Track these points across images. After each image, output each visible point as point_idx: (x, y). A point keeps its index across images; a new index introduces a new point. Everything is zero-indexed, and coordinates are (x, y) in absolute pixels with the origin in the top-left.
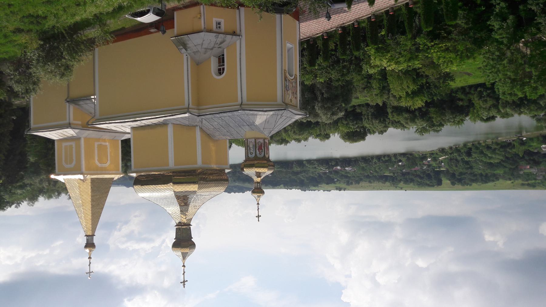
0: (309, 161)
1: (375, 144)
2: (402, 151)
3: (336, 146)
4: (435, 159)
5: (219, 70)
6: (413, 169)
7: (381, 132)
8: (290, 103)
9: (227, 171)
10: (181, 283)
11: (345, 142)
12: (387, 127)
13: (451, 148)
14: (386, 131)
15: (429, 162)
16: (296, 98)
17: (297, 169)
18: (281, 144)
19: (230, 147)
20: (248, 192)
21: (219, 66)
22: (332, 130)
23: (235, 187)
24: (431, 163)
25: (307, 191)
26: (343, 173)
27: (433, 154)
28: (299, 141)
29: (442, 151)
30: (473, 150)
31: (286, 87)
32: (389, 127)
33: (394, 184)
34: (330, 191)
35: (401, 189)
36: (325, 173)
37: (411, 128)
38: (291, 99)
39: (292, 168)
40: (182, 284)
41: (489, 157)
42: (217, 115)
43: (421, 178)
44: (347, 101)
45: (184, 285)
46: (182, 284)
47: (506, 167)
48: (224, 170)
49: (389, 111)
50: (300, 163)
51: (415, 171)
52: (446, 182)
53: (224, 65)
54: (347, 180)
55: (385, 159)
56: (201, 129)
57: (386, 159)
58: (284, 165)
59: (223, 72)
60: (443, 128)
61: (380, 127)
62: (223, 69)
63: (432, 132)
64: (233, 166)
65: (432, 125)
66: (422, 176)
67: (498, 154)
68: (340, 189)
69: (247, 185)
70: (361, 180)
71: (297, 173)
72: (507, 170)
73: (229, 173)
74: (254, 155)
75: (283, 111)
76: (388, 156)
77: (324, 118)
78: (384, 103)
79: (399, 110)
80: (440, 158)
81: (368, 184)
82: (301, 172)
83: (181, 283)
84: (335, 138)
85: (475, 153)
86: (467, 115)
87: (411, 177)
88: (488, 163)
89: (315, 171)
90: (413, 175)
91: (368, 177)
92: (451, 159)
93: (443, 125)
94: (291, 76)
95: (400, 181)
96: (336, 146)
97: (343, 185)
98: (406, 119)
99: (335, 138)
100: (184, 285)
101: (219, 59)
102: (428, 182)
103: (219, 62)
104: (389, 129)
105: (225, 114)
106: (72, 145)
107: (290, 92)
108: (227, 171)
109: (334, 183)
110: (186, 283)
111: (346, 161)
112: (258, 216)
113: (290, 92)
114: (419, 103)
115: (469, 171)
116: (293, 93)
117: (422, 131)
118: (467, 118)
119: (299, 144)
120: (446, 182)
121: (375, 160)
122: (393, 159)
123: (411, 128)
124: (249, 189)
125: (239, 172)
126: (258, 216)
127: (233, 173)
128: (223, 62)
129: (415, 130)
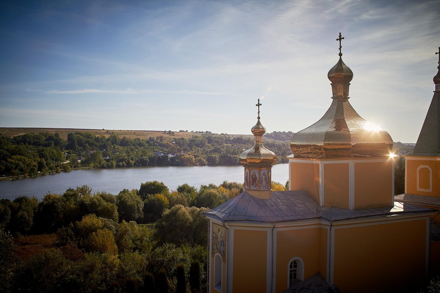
0: (202, 164)
1: (129, 180)
2: (195, 167)
3: (172, 178)
4: (74, 161)
5: (295, 266)
6: (95, 151)
7: (125, 191)
8: (220, 227)
9: (292, 156)
10: (343, 38)
11: (162, 183)
12: (119, 197)
13: (57, 172)
14: (121, 192)
15: (80, 159)
16: (213, 233)
17: (216, 156)
18: (231, 184)
19: (287, 183)
20: (269, 133)
21: (295, 271)
22: (175, 197)
23: (283, 139)
24: (78, 158)
25: (205, 131)
26: (166, 149)
27: (75, 167)
28: (211, 186)
29: (65, 169)
30: (36, 168)
31: (224, 245)
32: (117, 196)
33: (115, 137)
34: (181, 131)
35: (108, 132)
36: (185, 150)
37: (96, 194)
38: (219, 231)
39: (221, 157)
40: (342, 37)
41: (21, 161)
42: (300, 217)
43: (88, 142)
44: (160, 227)
45: (340, 36)
46: (342, 37)
47: (7, 150)
48: (295, 157)
49: (116, 214)
50: (212, 163)
51: (93, 150)
52: (64, 138)
53: (291, 271)
54: (162, 143)
55: (123, 164)
56: (318, 204)
57: (121, 164)
58: (228, 161)
59: (292, 263)
60: (65, 192)
61: (125, 196)
62: (291, 267)
63: (75, 189)
64: (284, 161)
65: (75, 195)
66: (87, 144)
67: (13, 164)
68: (170, 133)
69: (270, 141)
70: (148, 142)
71: (216, 150)
72: (5, 147)
73: (290, 154)
74: (262, 173)
75: (227, 219)
76: (118, 167)
77: (185, 210)
78: (120, 222)
79: (106, 213)
80: (68, 162)
81: (128, 137)
82: (211, 152)
83: (343, 38)
84: (172, 187)
85: (35, 166)
86: (41, 204)
87: (97, 144)
88: (22, 155)
89: (195, 153)
90: (95, 145)
91: (141, 145)
92: (57, 160)
93: (65, 195)
94: (218, 256)
95: (108, 140)
96: (172, 178)
97: (165, 136)
98: (100, 205)
99: (172, 187)
100: (340, 36)
101: (295, 277)
102: (81, 137)
103: (295, 274)
104: (117, 194)
105: (292, 218)
106: (318, 165)
107: (220, 239)
108: (292, 156)
109: (175, 140)
110: (338, 38)
111: (161, 162)
112: (259, 105)
113: (220, 239)
114: (90, 220)
115: (40, 148)
116: (217, 238)
117: (84, 190)
118: (41, 201)
119: (211, 183)
120: (64, 138)
121: (133, 162)
122: (115, 163)
123: (96, 194)
124: (269, 136)
125: (279, 155)
126: (259, 105)
127: (284, 154)
128: (291, 275)
129: (92, 193)
